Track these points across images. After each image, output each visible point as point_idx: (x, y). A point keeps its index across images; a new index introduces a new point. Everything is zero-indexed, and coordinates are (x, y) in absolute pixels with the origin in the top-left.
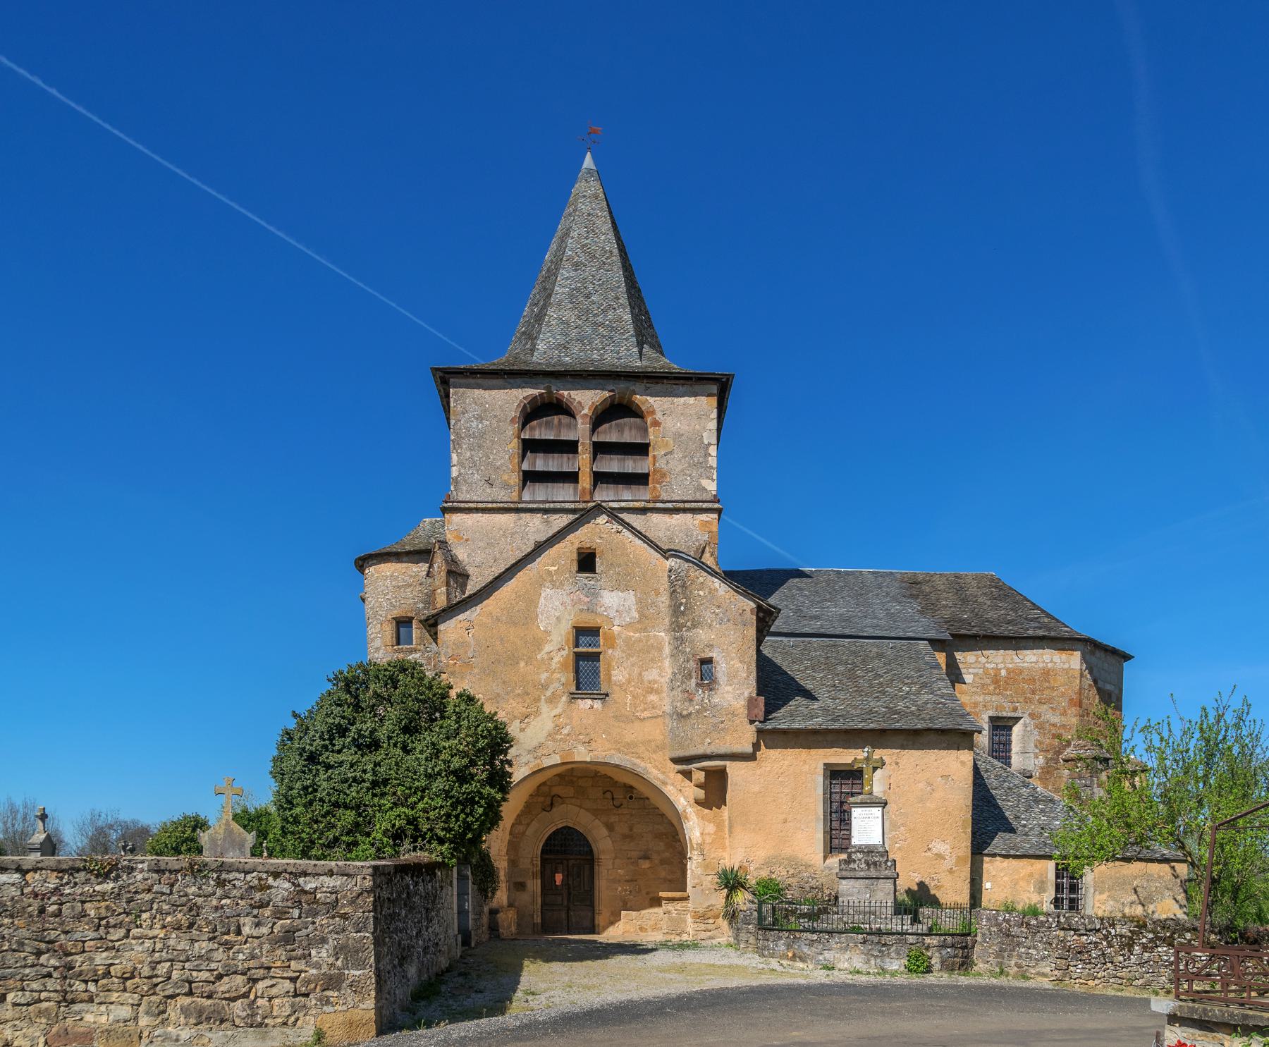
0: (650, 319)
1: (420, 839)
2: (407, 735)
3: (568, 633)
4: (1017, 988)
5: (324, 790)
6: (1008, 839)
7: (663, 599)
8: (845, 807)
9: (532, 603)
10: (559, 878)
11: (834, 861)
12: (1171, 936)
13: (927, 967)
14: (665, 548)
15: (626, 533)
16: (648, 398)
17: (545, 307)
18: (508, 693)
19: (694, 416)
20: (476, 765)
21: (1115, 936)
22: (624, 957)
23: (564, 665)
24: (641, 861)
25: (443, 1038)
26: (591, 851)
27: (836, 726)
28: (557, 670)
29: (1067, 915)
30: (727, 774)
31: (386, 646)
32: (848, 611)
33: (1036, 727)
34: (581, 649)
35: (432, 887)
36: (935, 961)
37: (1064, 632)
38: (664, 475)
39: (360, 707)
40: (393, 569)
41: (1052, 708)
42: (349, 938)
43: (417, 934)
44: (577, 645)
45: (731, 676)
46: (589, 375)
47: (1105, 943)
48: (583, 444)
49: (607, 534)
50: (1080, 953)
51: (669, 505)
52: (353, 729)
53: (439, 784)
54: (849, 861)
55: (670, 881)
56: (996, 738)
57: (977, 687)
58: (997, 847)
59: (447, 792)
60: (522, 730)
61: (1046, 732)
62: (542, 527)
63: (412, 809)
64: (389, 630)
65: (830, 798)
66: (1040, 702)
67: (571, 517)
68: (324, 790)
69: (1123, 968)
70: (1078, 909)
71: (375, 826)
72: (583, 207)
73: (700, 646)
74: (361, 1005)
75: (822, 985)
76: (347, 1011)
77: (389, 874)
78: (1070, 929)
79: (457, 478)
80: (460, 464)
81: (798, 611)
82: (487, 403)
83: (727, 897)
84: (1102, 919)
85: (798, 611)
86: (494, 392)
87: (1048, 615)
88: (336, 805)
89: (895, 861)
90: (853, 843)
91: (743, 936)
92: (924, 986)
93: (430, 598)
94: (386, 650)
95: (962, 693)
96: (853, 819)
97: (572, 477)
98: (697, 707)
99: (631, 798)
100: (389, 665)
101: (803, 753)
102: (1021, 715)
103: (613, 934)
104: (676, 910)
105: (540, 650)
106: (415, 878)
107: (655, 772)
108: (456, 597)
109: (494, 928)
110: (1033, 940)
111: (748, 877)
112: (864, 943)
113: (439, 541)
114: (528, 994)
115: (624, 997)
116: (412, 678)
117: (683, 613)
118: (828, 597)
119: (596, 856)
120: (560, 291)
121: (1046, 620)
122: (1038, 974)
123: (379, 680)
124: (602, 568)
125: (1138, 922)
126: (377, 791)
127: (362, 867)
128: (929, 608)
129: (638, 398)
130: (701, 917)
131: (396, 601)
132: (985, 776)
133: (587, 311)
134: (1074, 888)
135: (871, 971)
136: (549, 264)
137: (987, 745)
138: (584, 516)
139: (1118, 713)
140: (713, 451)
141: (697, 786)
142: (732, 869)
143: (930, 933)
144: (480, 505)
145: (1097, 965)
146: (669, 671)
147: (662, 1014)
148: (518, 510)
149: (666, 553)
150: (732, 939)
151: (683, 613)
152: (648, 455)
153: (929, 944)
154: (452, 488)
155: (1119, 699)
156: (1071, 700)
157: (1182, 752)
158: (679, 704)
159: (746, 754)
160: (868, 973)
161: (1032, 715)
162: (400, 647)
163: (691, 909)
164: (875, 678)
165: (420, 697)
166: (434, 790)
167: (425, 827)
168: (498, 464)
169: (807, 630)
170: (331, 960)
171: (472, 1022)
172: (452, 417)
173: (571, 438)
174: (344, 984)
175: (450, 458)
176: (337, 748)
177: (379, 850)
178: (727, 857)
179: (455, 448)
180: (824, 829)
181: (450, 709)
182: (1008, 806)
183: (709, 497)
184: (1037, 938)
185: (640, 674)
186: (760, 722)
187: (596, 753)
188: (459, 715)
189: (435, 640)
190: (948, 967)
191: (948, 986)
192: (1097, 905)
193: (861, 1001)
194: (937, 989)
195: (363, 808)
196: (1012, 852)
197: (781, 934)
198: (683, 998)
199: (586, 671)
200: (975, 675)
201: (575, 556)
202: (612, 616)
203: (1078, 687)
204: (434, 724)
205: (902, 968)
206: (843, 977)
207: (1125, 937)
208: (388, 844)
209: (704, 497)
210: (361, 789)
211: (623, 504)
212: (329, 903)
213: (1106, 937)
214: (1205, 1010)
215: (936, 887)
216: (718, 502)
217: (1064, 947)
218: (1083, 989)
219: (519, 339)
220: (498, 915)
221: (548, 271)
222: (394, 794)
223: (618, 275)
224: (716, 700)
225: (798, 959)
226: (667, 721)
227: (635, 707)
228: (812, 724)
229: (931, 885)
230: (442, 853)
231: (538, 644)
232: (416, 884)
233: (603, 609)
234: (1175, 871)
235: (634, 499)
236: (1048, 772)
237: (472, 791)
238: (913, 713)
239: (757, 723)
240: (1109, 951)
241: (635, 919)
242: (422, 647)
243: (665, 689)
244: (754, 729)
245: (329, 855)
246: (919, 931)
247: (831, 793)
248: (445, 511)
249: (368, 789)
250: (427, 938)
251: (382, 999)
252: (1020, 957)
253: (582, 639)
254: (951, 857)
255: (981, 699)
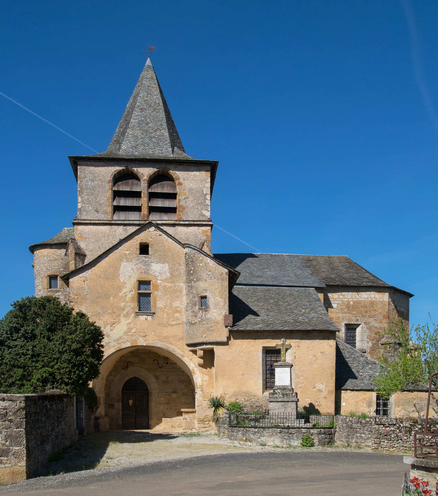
0: (178, 135)
1: (56, 383)
2: (50, 333)
3: (135, 284)
4: (355, 453)
5: (7, 359)
6: (354, 382)
7: (183, 267)
8: (273, 368)
9: (116, 268)
10: (131, 402)
11: (267, 393)
12: (430, 427)
13: (312, 444)
14: (183, 243)
15: (164, 236)
16: (176, 172)
17: (126, 128)
18: (104, 312)
19: (199, 181)
20: (85, 347)
21: (403, 427)
22: (161, 440)
23: (132, 299)
24: (172, 394)
25: (61, 480)
26: (147, 389)
27: (268, 329)
28: (129, 301)
29: (380, 418)
30: (214, 352)
31: (44, 289)
32: (276, 274)
33: (368, 328)
34: (141, 291)
35: (61, 406)
36: (316, 441)
37: (380, 284)
38: (184, 208)
39: (27, 319)
40: (48, 252)
41: (375, 320)
42: (13, 432)
43: (52, 429)
44: (139, 289)
45: (216, 305)
46: (147, 161)
47: (398, 431)
48: (144, 193)
49: (154, 236)
50: (386, 435)
51: (187, 223)
52: (23, 329)
53: (65, 356)
54: (273, 394)
55: (187, 403)
56: (348, 334)
57: (339, 310)
58: (348, 386)
59: (70, 360)
60: (111, 330)
61: (373, 331)
62: (123, 232)
63: (52, 368)
64: (46, 281)
65: (266, 363)
66: (369, 316)
67: (137, 228)
68: (7, 359)
69: (406, 442)
70: (387, 415)
71: (33, 376)
72: (146, 83)
73: (200, 290)
74: (18, 464)
75: (258, 453)
76: (11, 467)
77: (35, 400)
78: (381, 424)
79: (80, 208)
80: (82, 202)
81: (251, 273)
82: (96, 173)
83: (214, 411)
84: (396, 419)
85: (251, 273)
86: (100, 168)
87: (374, 276)
88: (14, 366)
89: (297, 393)
90: (276, 385)
91: (222, 430)
92: (309, 453)
93: (67, 265)
94: (44, 291)
95: (332, 312)
96: (276, 373)
97: (138, 209)
98: (199, 319)
99: (167, 363)
100: (42, 298)
101: (252, 342)
102: (360, 323)
103: (157, 429)
104: (189, 417)
105: (120, 291)
106: (51, 402)
107: (178, 351)
108: (79, 265)
109: (97, 426)
110: (363, 430)
111: (225, 401)
112: (281, 432)
113: (71, 239)
114: (108, 459)
115: (156, 460)
116: (54, 305)
117: (192, 274)
118: (266, 267)
119: (150, 391)
120: (133, 121)
121: (372, 278)
122: (366, 446)
123: (36, 306)
124: (152, 252)
125: (414, 420)
126: (34, 359)
127: (20, 397)
128: (315, 272)
129: (171, 172)
130: (202, 421)
131: (49, 267)
132: (343, 352)
133: (147, 131)
134: (385, 405)
135: (284, 446)
136: (129, 109)
137: (344, 337)
138: (143, 227)
139: (407, 322)
140: (208, 197)
141: (200, 358)
142: (217, 398)
143: (314, 427)
144: (92, 222)
145: (394, 441)
146: (186, 302)
147: (174, 468)
148: (111, 224)
149: (184, 246)
150: (217, 432)
151: (192, 274)
152: (176, 199)
153: (313, 433)
154: (78, 213)
155: (408, 315)
156: (384, 316)
157: (434, 340)
158: (190, 318)
159: (224, 342)
160: (283, 447)
161: (366, 323)
162: (51, 289)
163: (197, 417)
164: (288, 306)
165: (57, 314)
166: (63, 359)
167: (58, 377)
168: (101, 202)
169: (255, 283)
170: (3, 442)
171: (77, 472)
172: (78, 180)
173: (138, 190)
174: (10, 454)
175: (77, 199)
176: (14, 338)
177: (35, 388)
178: (215, 392)
179: (80, 194)
180: (263, 378)
181: (72, 320)
182: (354, 367)
183: (206, 219)
184: (365, 429)
185: (171, 304)
186: (231, 327)
187: (149, 341)
188: (76, 324)
189: (68, 286)
190: (322, 443)
191: (321, 453)
192: (397, 412)
193: (276, 461)
194: (315, 454)
195: (27, 368)
196: (355, 388)
197: (240, 429)
198: (187, 460)
199: (144, 302)
200: (338, 304)
201: (138, 246)
202: (157, 275)
203: (387, 310)
204: (64, 327)
205: (300, 445)
206: (270, 449)
207: (407, 427)
208: (39, 386)
209: (204, 219)
210: (26, 358)
211: (163, 222)
212: (2, 414)
213: (398, 428)
214: (427, 462)
215: (318, 405)
216: (211, 221)
217: (378, 433)
218: (388, 453)
219: (113, 143)
220: (99, 420)
221: (128, 112)
222: (43, 361)
223: (162, 114)
224: (208, 316)
225: (248, 441)
226: (184, 326)
227: (169, 320)
228: (256, 328)
229: (315, 404)
230: (67, 390)
231: (120, 288)
232: (52, 405)
233: (152, 272)
234: (433, 396)
235: (169, 219)
236: (373, 350)
237: (82, 360)
238: (306, 322)
239: (229, 327)
240: (400, 434)
241: (169, 422)
242: (62, 290)
243: (183, 310)
244: (228, 330)
245: (10, 390)
246: (308, 427)
247: (266, 361)
248: (74, 224)
249: (30, 358)
250: (58, 431)
251: (30, 461)
252: (357, 438)
253: (142, 286)
254: (325, 391)
255: (341, 315)
